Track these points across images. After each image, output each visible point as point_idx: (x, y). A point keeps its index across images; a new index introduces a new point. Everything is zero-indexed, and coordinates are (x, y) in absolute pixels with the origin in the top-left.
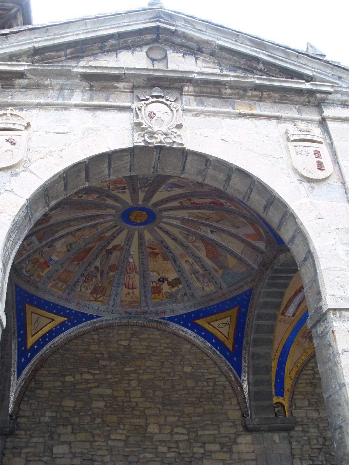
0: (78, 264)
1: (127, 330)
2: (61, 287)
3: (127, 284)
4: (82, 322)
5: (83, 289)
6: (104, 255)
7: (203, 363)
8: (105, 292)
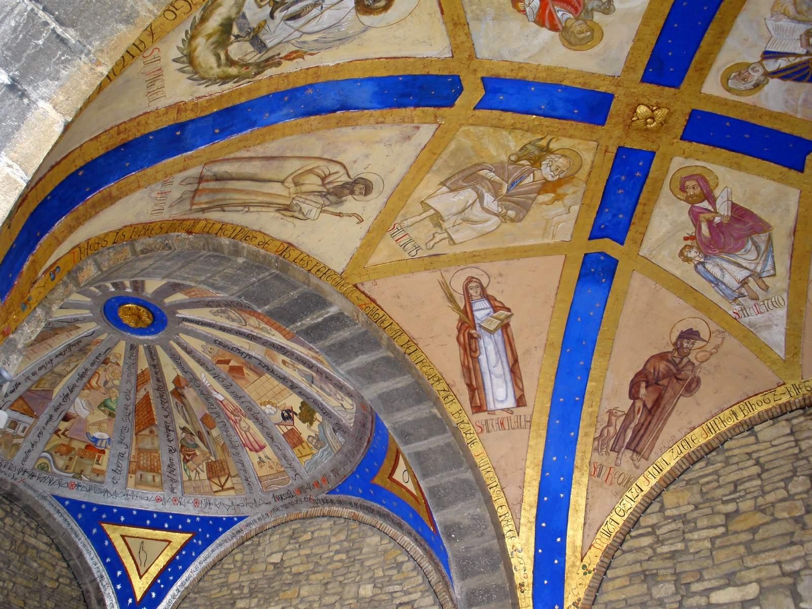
0: (151, 432)
1: (283, 533)
2: (154, 480)
3: (248, 444)
4: (218, 534)
5: (193, 475)
6: (176, 403)
7: (394, 572)
8: (228, 469)
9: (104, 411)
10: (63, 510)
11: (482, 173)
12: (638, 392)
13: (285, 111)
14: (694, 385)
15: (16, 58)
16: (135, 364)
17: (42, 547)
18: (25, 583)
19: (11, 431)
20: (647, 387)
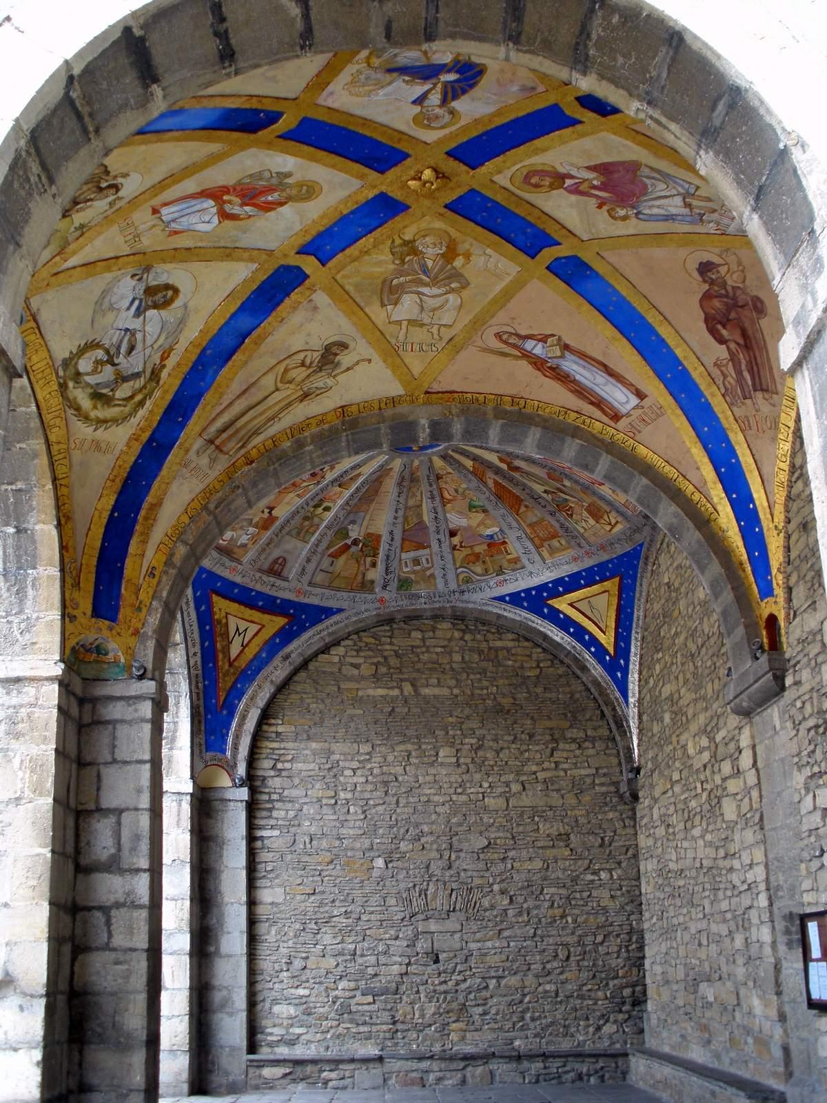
0: (526, 506)
9: (477, 512)
10: (508, 607)
11: (395, 282)
12: (722, 336)
13: (211, 372)
14: (759, 305)
15: (9, 516)
16: (465, 467)
17: (510, 644)
18: (506, 682)
19: (419, 568)
20: (724, 327)
